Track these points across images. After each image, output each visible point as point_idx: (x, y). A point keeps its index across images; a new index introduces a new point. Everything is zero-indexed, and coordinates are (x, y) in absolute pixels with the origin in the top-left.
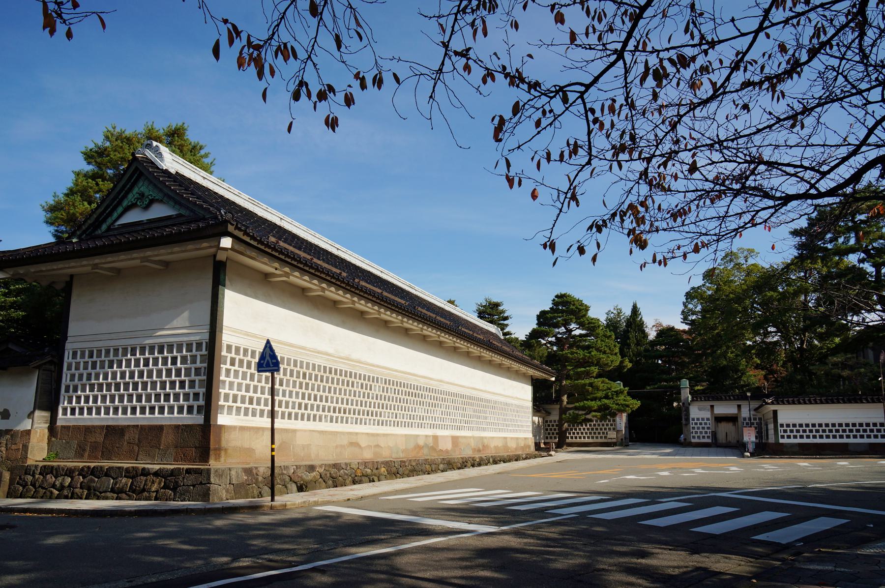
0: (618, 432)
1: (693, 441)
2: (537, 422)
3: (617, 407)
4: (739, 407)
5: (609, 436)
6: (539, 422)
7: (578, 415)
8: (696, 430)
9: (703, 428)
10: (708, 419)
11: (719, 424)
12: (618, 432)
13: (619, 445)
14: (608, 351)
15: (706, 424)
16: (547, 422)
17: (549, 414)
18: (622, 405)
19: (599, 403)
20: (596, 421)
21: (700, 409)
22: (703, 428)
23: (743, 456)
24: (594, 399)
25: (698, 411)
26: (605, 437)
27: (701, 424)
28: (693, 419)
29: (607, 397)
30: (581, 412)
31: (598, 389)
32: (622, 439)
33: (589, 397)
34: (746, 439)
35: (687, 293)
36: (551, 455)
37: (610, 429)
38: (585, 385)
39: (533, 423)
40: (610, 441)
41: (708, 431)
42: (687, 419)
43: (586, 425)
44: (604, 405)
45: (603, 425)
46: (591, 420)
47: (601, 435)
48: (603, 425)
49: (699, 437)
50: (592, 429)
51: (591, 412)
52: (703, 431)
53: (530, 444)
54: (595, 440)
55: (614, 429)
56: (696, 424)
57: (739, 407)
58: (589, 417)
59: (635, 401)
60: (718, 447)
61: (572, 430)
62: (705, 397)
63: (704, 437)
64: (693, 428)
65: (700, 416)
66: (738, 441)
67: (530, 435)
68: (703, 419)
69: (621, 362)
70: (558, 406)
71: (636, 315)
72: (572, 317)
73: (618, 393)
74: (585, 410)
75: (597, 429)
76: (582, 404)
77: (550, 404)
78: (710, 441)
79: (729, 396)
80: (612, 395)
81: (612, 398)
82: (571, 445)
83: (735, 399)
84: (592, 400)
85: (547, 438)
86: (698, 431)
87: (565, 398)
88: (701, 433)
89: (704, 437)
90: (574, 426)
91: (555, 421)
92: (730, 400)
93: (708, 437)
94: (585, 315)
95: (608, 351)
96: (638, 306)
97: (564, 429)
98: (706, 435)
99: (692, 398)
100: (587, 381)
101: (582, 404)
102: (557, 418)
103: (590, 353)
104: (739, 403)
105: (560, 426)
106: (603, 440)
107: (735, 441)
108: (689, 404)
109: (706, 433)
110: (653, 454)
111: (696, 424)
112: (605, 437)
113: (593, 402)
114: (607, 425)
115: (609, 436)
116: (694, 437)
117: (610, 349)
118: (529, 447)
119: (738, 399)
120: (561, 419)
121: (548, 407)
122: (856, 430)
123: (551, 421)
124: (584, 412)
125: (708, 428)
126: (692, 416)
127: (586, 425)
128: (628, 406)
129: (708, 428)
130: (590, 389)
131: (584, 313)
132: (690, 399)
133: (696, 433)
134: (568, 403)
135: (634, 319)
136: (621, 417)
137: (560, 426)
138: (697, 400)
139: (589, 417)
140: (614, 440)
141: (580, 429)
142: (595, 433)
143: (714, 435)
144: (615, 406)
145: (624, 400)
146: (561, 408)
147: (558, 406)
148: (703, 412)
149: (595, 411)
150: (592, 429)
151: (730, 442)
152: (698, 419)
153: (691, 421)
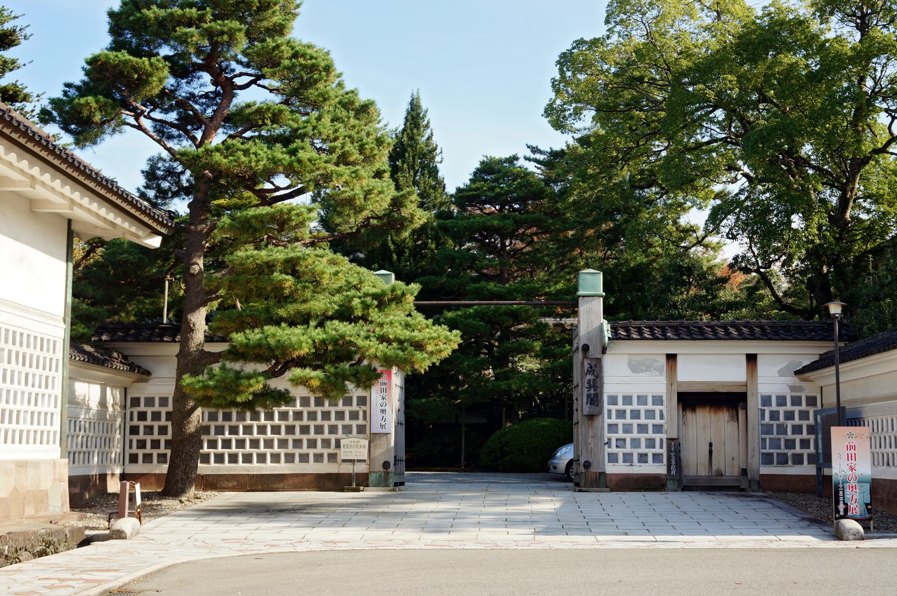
0: (374, 438)
1: (611, 469)
2: (94, 404)
3: (383, 347)
4: (752, 359)
5: (343, 454)
6: (103, 403)
7: (238, 375)
8: (621, 435)
9: (642, 428)
10: (658, 400)
11: (689, 415)
12: (374, 438)
13: (377, 485)
14: (355, 156)
15: (650, 414)
16: (136, 402)
17: (146, 374)
18: (400, 342)
19: (318, 334)
20: (305, 402)
21: (635, 368)
22: (642, 428)
23: (839, 536)
24: (303, 319)
25: (628, 372)
26: (333, 457)
27: (636, 414)
28: (613, 400)
29: (345, 314)
30: (250, 367)
31: (316, 282)
32: (386, 465)
33: (282, 312)
34: (839, 468)
35: (563, 55)
36: (119, 535)
37: (347, 430)
38: (270, 266)
39: (71, 401)
40: (346, 469)
41: (657, 437)
42: (595, 400)
43: (270, 417)
44: (335, 341)
45: (326, 416)
46: (283, 398)
47: (312, 435)
48: (326, 416)
49: (628, 458)
50: (290, 430)
51: (286, 367)
52: (643, 437)
53: (46, 484)
54: (297, 468)
55: (361, 429)
56: (621, 414)
57: (752, 359)
58: (279, 384)
59: (442, 331)
60: (685, 489)
61: (220, 430)
62: (651, 329)
63: (643, 458)
64: (613, 428)
65: (634, 391)
66: (744, 472)
67: (52, 452)
68: (642, 400)
69: (397, 203)
70: (175, 349)
71: (417, 126)
72: (235, 24)
73: (382, 301)
74: (268, 360)
75: (305, 430)
76: (255, 336)
77: (149, 340)
78: (660, 469)
79: (725, 327)
80: (366, 307)
81: (365, 318)
82: (212, 483)
83: (742, 337)
84: (292, 323)
85: (134, 459)
86: (628, 437)
87: (199, 319)
88: (636, 443)
89: (643, 458)
90: (227, 417)
91: (164, 402)
92: (728, 337)
93: (657, 458)
94: (279, 30)
95: (355, 156)
96: (424, 104)
97: (191, 428)
98: (650, 452)
99: (614, 329)
100: (279, 254)
101: (255, 336)
102: (169, 390)
103: (293, 152)
104: (752, 347)
105: (179, 416)
106: (326, 468)
107: (736, 472)
108: (604, 350)
109: (651, 443)
110: (508, 522)
111: (621, 414)
112: (333, 457)
113: (298, 330)
114: (340, 415)
115: (343, 454)
116: (613, 458)
117: (361, 149)
118: (41, 498)
119: (753, 337)
120: (181, 395)
121: (142, 350)
122: (638, 417)
123: (150, 402)
124: (262, 367)
125: (658, 429)
126: (609, 389)
127: (270, 417)
128: (419, 346)
129: (658, 429)
130: (289, 281)
131: (277, 19)
132: (607, 334)
133: (621, 442)
134: (209, 339)
135: (411, 138)
136: (386, 390)
137: (179, 416)
138: (629, 338)
139: (279, 384)
140: (361, 468)
141: (248, 430)
142: (298, 443)
143: (675, 447)
144: (375, 348)
145: (407, 326)
146: (183, 355)
147: (175, 349)
148: (643, 377)
149: (301, 362)
150: (290, 430)
151: (720, 474)
152: (627, 400)
153: (606, 407)
